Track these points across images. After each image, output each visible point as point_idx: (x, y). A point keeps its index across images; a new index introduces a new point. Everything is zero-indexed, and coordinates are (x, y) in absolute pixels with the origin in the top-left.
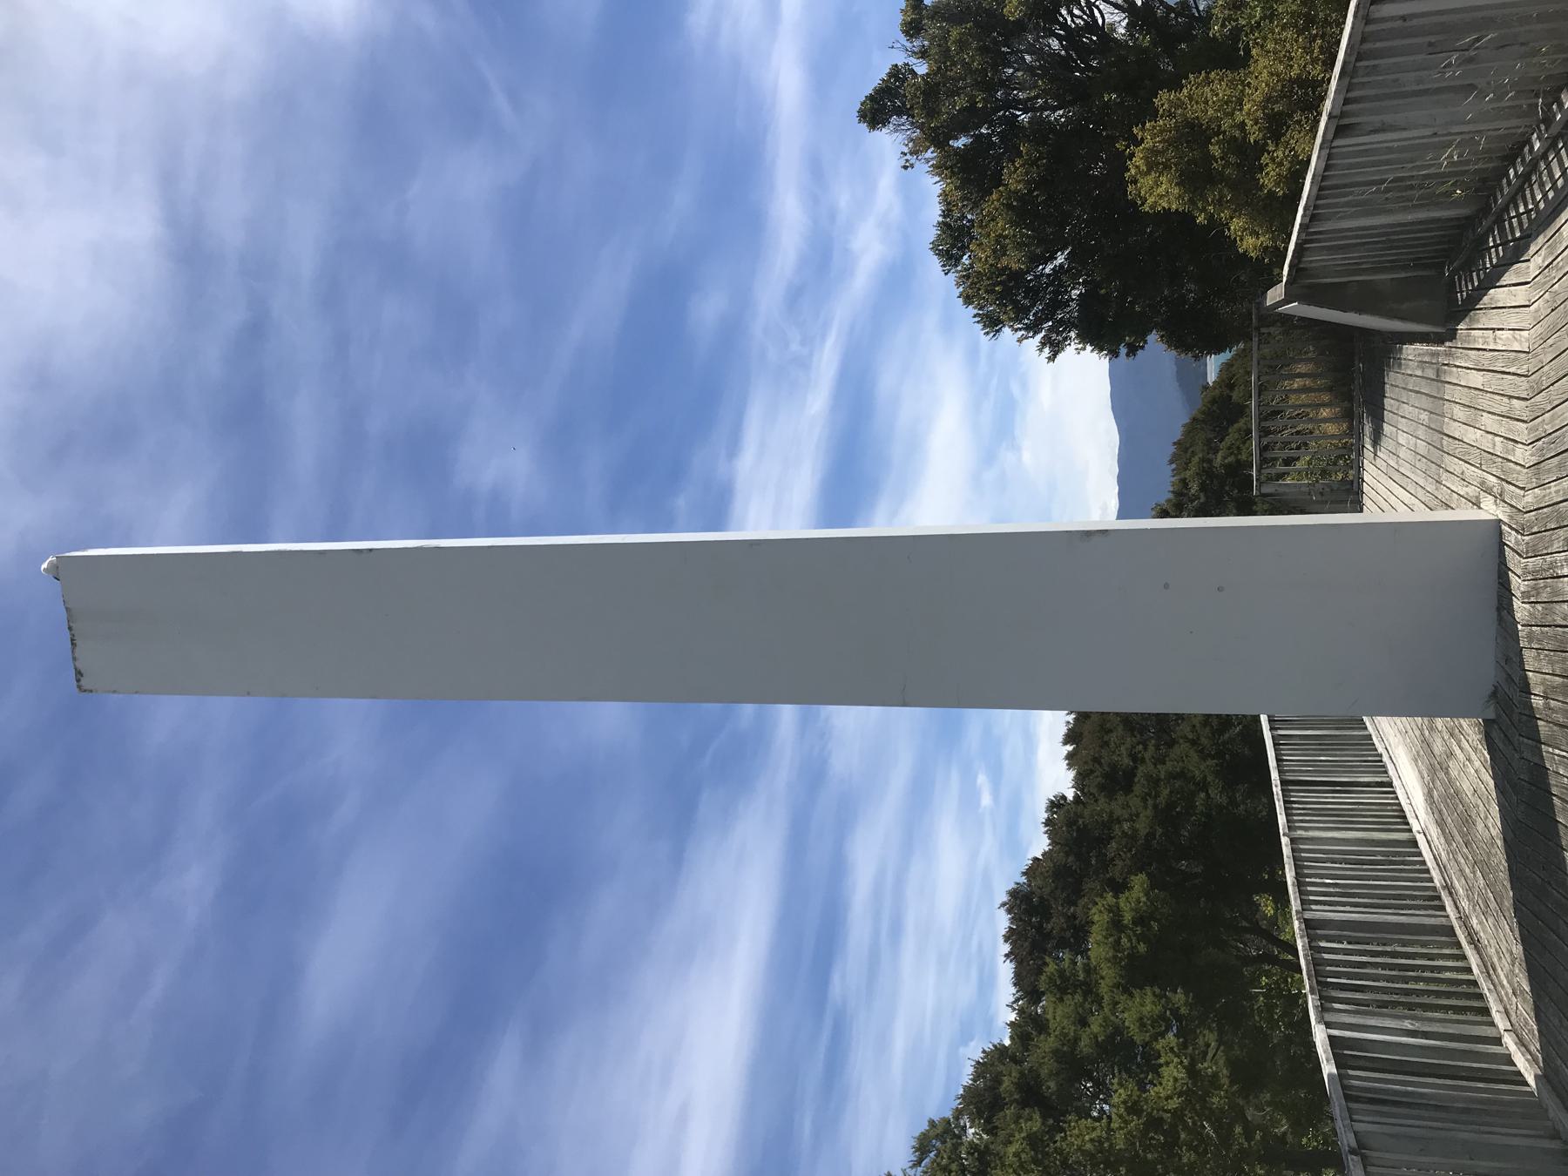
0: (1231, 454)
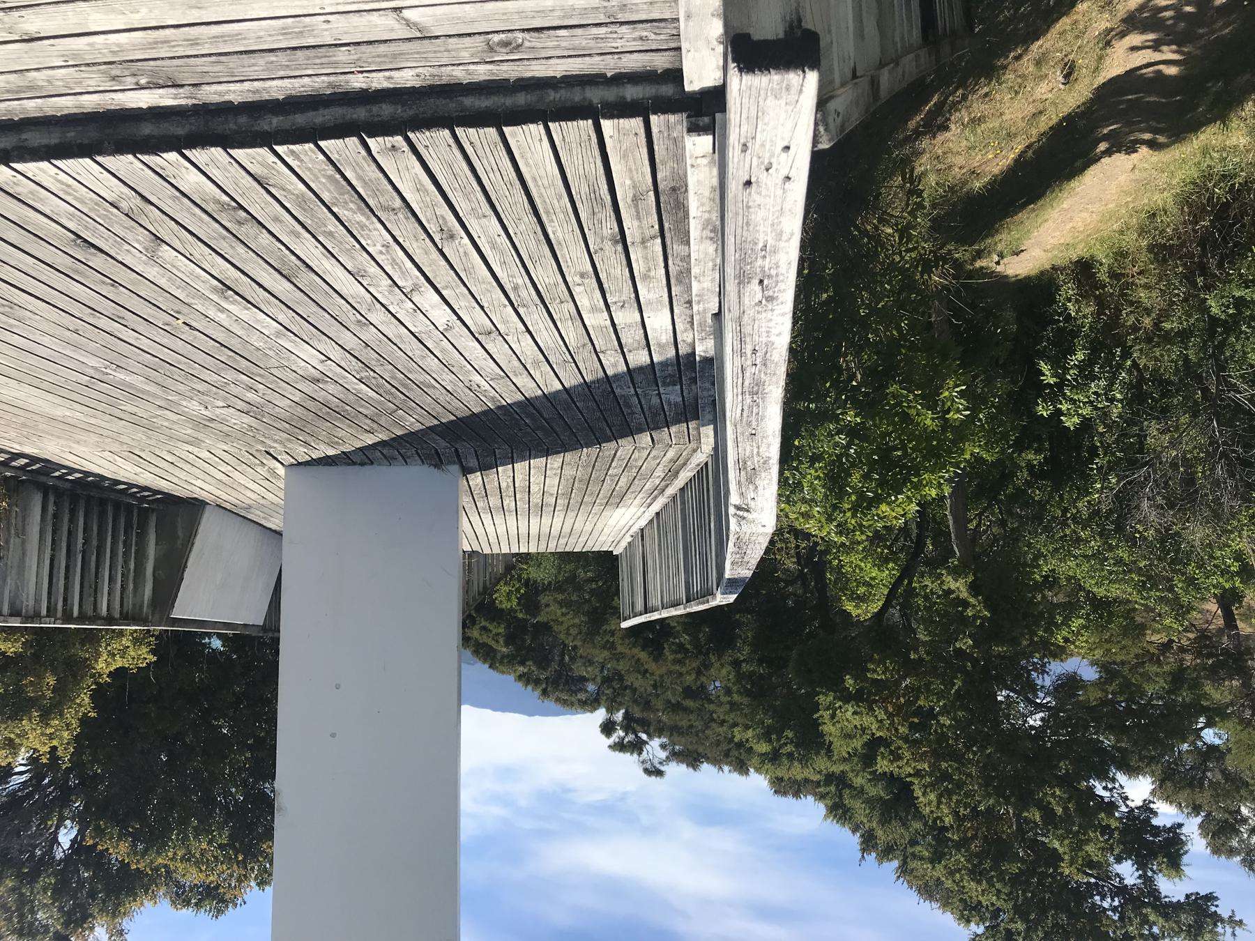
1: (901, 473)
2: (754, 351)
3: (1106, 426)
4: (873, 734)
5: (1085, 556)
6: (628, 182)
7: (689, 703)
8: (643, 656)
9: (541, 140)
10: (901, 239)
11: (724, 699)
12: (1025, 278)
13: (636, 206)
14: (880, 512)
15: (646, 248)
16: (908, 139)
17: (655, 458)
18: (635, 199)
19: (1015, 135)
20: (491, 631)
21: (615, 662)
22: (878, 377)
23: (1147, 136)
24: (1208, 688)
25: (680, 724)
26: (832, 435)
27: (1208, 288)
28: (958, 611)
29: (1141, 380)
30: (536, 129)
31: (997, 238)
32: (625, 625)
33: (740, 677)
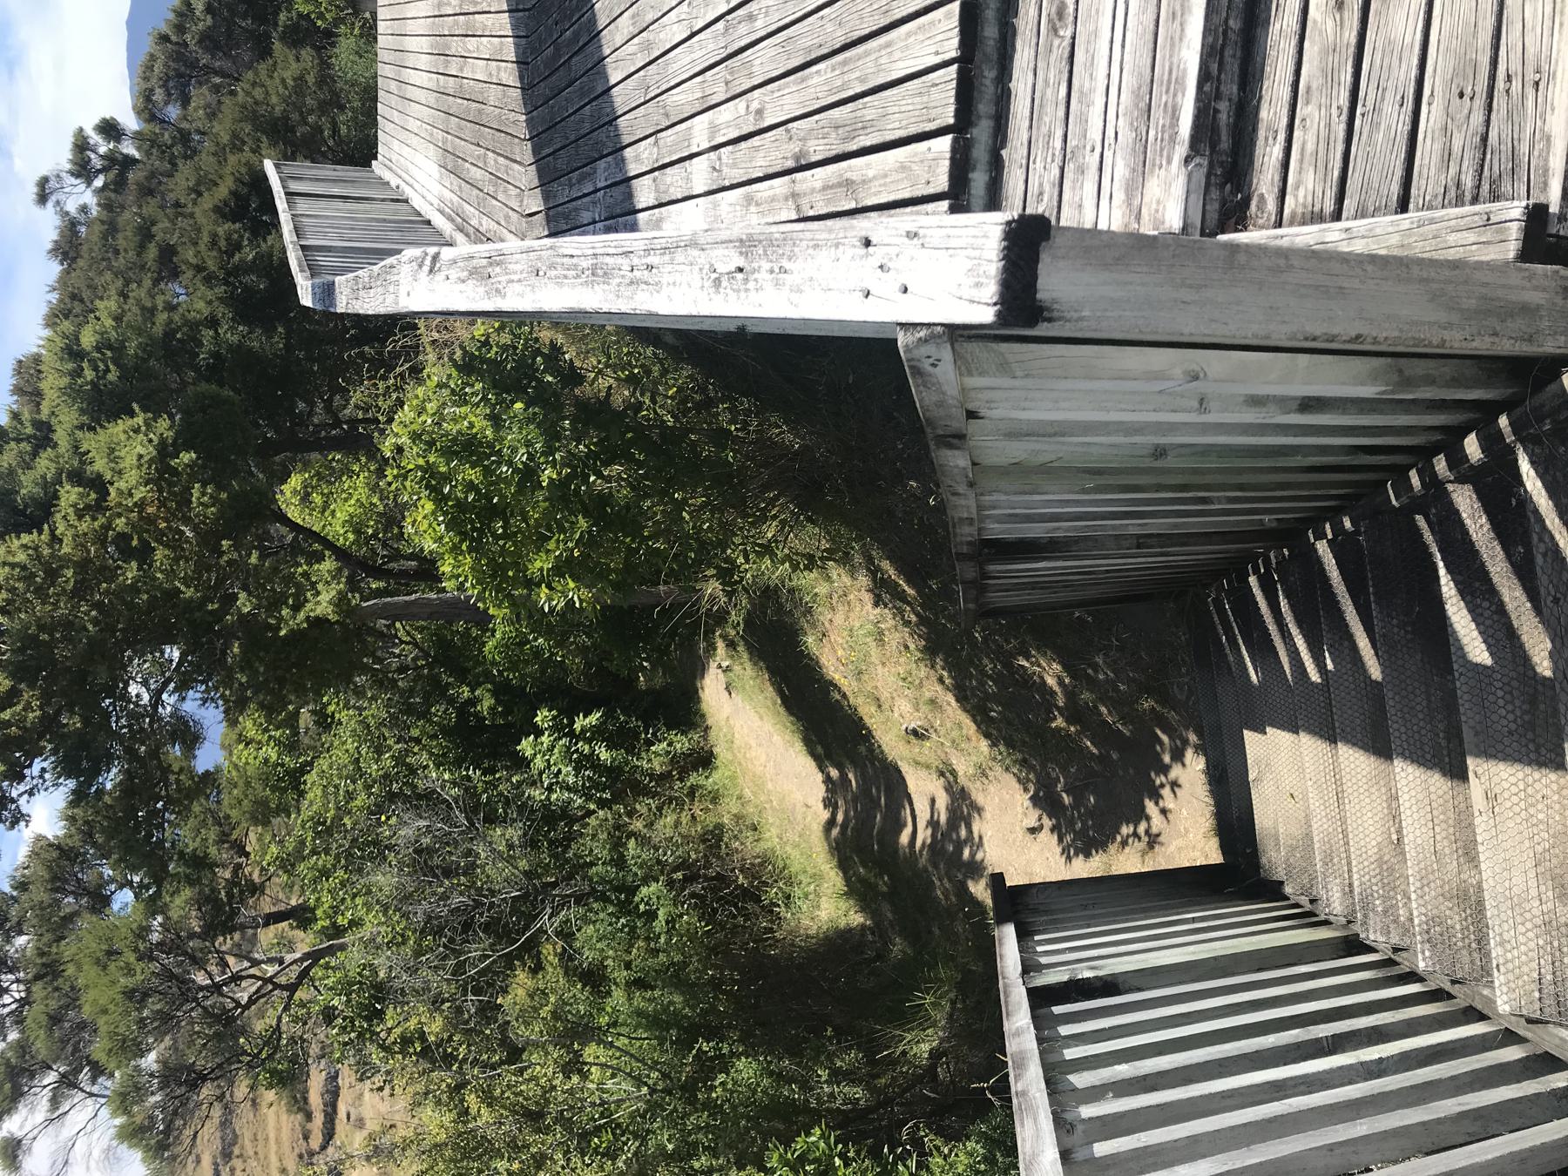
1: (474, 529)
2: (650, 267)
3: (520, 783)
4: (112, 484)
5: (357, 760)
6: (871, 173)
7: (152, 252)
8: (223, 191)
9: (937, 53)
10: (760, 545)
11: (160, 300)
12: (699, 698)
13: (840, 185)
14: (422, 502)
15: (786, 199)
16: (870, 560)
17: (507, 217)
18: (848, 183)
19: (859, 680)
21: (213, 149)
22: (597, 507)
23: (840, 817)
24: (187, 893)
25: (120, 236)
26: (527, 446)
27: (670, 884)
28: (288, 598)
29: (572, 820)
30: (951, 48)
31: (748, 665)
32: (269, 166)
33: (194, 326)
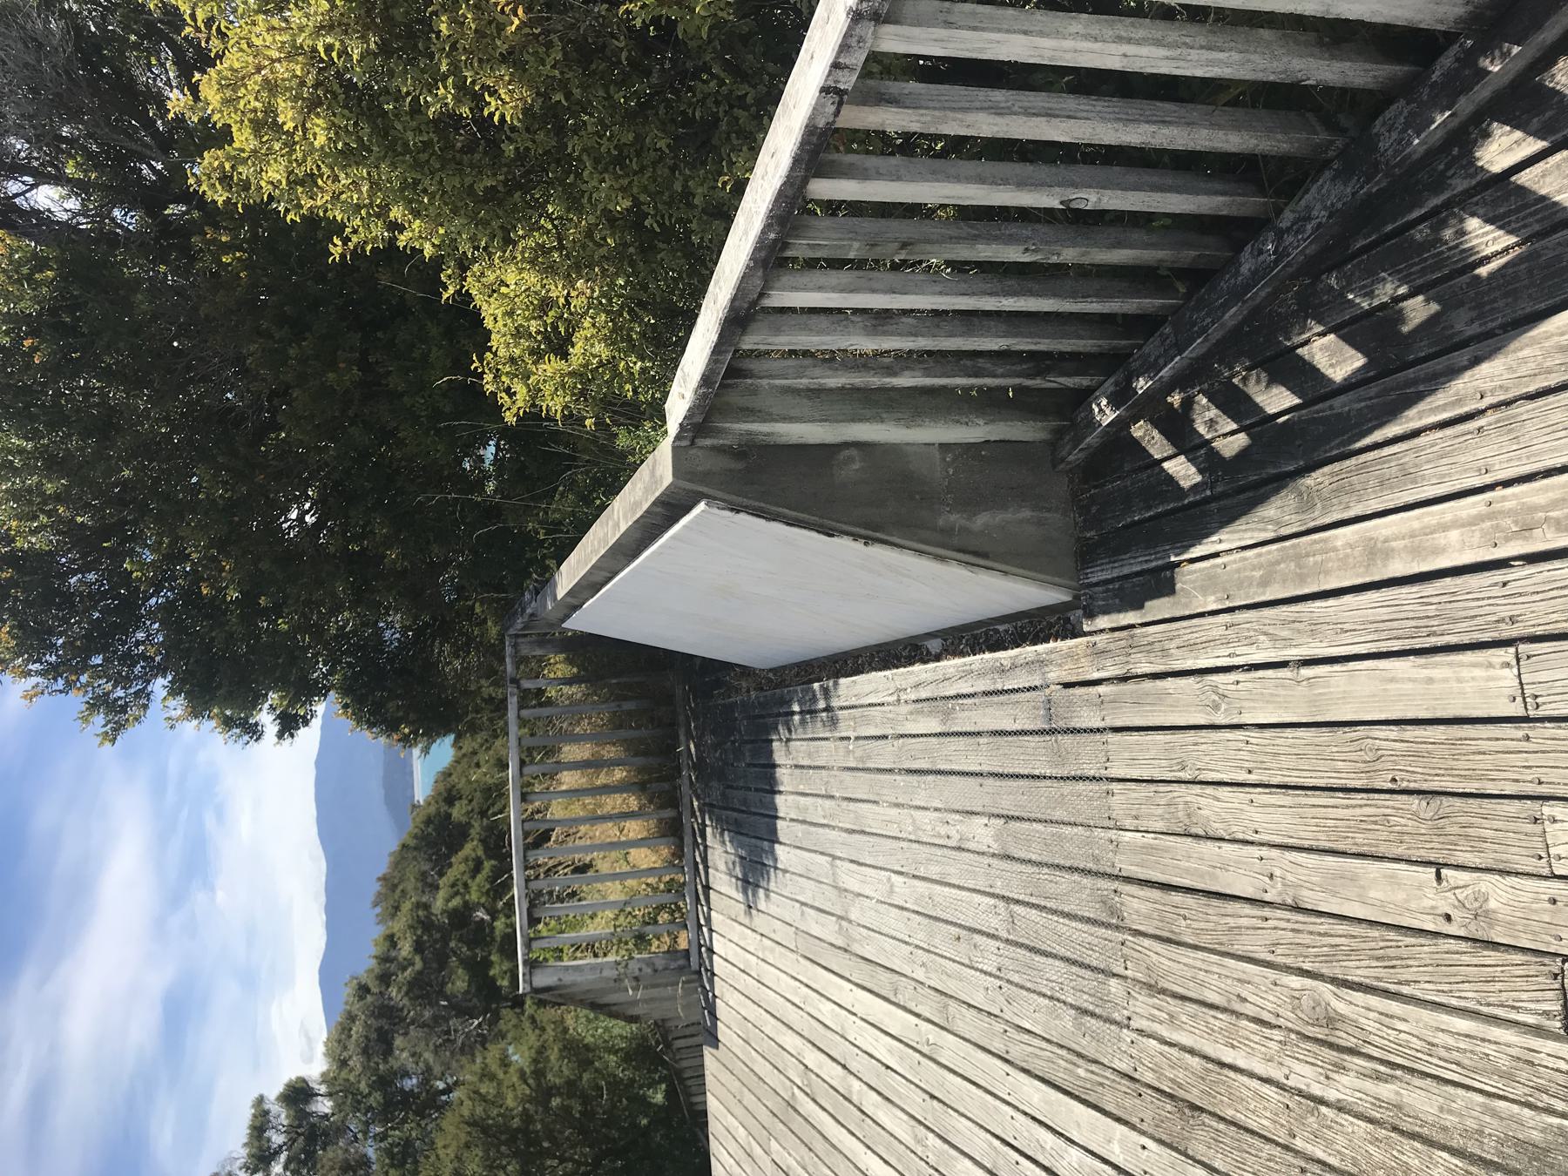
0: (457, 893)
20: (473, 877)
